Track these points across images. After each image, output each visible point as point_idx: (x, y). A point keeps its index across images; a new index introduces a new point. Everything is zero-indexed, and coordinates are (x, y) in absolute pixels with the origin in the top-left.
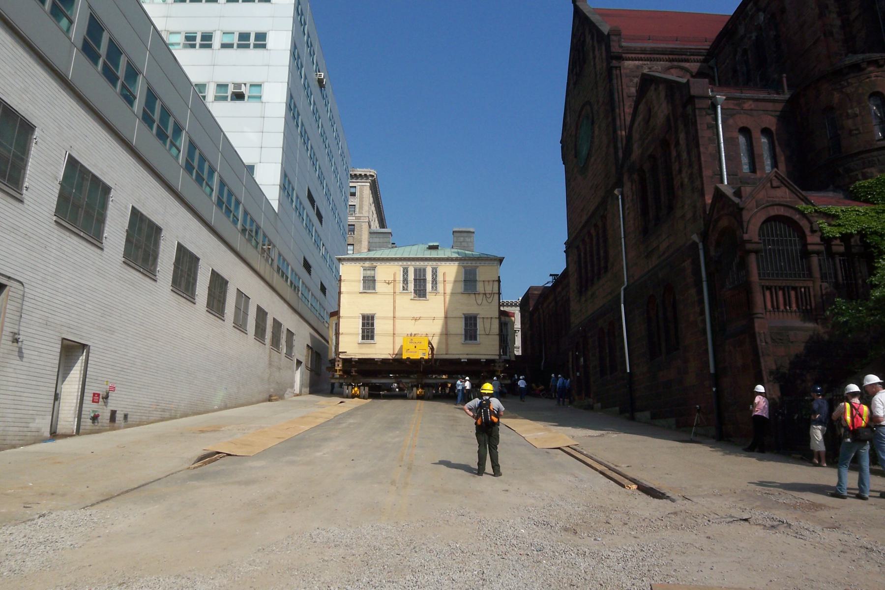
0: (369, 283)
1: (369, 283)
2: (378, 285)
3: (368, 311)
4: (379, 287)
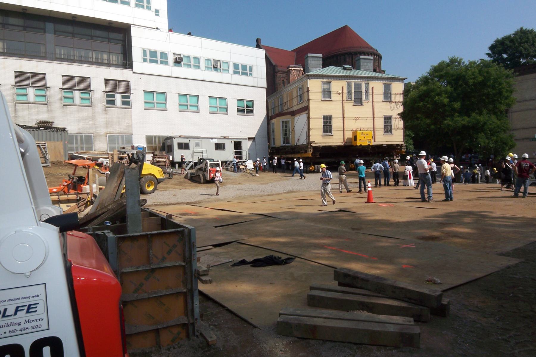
0: (327, 94)
1: (327, 94)
2: (333, 95)
3: (327, 114)
4: (334, 96)
